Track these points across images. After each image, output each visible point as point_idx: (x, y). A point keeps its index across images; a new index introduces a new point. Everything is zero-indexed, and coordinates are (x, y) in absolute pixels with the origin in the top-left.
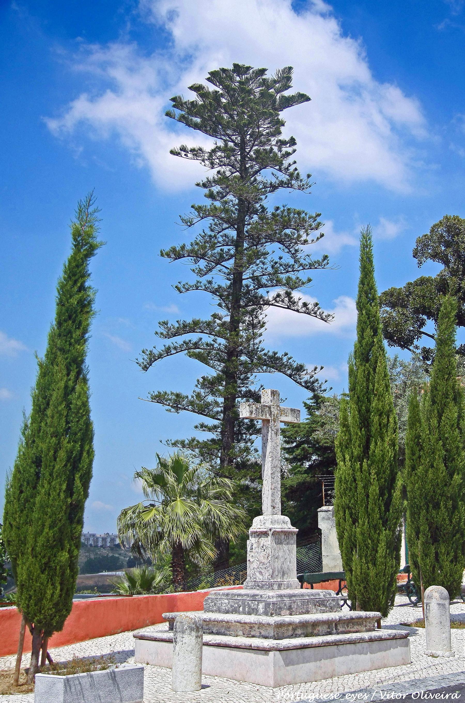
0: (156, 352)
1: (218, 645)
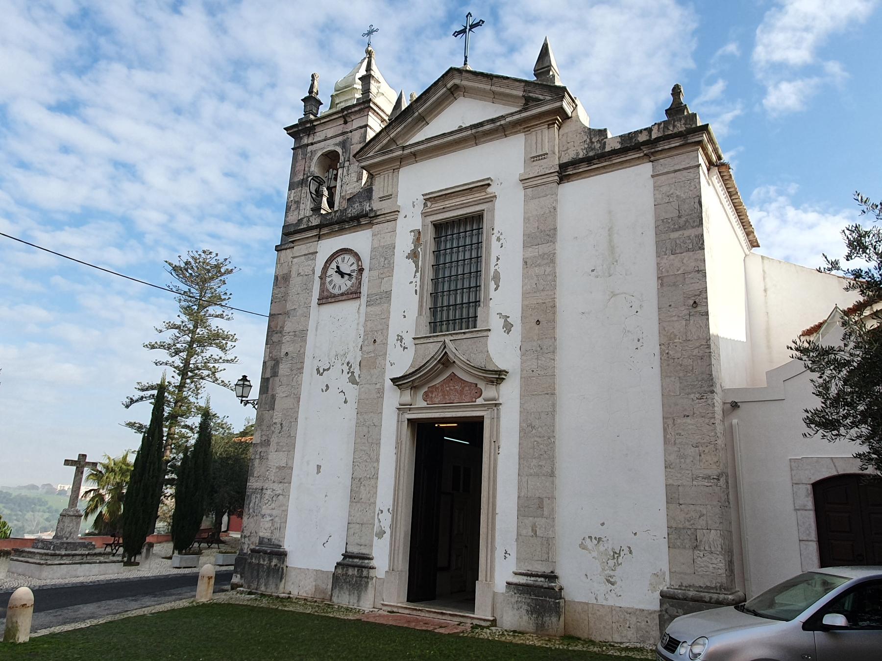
0: (134, 399)
1: (383, 111)
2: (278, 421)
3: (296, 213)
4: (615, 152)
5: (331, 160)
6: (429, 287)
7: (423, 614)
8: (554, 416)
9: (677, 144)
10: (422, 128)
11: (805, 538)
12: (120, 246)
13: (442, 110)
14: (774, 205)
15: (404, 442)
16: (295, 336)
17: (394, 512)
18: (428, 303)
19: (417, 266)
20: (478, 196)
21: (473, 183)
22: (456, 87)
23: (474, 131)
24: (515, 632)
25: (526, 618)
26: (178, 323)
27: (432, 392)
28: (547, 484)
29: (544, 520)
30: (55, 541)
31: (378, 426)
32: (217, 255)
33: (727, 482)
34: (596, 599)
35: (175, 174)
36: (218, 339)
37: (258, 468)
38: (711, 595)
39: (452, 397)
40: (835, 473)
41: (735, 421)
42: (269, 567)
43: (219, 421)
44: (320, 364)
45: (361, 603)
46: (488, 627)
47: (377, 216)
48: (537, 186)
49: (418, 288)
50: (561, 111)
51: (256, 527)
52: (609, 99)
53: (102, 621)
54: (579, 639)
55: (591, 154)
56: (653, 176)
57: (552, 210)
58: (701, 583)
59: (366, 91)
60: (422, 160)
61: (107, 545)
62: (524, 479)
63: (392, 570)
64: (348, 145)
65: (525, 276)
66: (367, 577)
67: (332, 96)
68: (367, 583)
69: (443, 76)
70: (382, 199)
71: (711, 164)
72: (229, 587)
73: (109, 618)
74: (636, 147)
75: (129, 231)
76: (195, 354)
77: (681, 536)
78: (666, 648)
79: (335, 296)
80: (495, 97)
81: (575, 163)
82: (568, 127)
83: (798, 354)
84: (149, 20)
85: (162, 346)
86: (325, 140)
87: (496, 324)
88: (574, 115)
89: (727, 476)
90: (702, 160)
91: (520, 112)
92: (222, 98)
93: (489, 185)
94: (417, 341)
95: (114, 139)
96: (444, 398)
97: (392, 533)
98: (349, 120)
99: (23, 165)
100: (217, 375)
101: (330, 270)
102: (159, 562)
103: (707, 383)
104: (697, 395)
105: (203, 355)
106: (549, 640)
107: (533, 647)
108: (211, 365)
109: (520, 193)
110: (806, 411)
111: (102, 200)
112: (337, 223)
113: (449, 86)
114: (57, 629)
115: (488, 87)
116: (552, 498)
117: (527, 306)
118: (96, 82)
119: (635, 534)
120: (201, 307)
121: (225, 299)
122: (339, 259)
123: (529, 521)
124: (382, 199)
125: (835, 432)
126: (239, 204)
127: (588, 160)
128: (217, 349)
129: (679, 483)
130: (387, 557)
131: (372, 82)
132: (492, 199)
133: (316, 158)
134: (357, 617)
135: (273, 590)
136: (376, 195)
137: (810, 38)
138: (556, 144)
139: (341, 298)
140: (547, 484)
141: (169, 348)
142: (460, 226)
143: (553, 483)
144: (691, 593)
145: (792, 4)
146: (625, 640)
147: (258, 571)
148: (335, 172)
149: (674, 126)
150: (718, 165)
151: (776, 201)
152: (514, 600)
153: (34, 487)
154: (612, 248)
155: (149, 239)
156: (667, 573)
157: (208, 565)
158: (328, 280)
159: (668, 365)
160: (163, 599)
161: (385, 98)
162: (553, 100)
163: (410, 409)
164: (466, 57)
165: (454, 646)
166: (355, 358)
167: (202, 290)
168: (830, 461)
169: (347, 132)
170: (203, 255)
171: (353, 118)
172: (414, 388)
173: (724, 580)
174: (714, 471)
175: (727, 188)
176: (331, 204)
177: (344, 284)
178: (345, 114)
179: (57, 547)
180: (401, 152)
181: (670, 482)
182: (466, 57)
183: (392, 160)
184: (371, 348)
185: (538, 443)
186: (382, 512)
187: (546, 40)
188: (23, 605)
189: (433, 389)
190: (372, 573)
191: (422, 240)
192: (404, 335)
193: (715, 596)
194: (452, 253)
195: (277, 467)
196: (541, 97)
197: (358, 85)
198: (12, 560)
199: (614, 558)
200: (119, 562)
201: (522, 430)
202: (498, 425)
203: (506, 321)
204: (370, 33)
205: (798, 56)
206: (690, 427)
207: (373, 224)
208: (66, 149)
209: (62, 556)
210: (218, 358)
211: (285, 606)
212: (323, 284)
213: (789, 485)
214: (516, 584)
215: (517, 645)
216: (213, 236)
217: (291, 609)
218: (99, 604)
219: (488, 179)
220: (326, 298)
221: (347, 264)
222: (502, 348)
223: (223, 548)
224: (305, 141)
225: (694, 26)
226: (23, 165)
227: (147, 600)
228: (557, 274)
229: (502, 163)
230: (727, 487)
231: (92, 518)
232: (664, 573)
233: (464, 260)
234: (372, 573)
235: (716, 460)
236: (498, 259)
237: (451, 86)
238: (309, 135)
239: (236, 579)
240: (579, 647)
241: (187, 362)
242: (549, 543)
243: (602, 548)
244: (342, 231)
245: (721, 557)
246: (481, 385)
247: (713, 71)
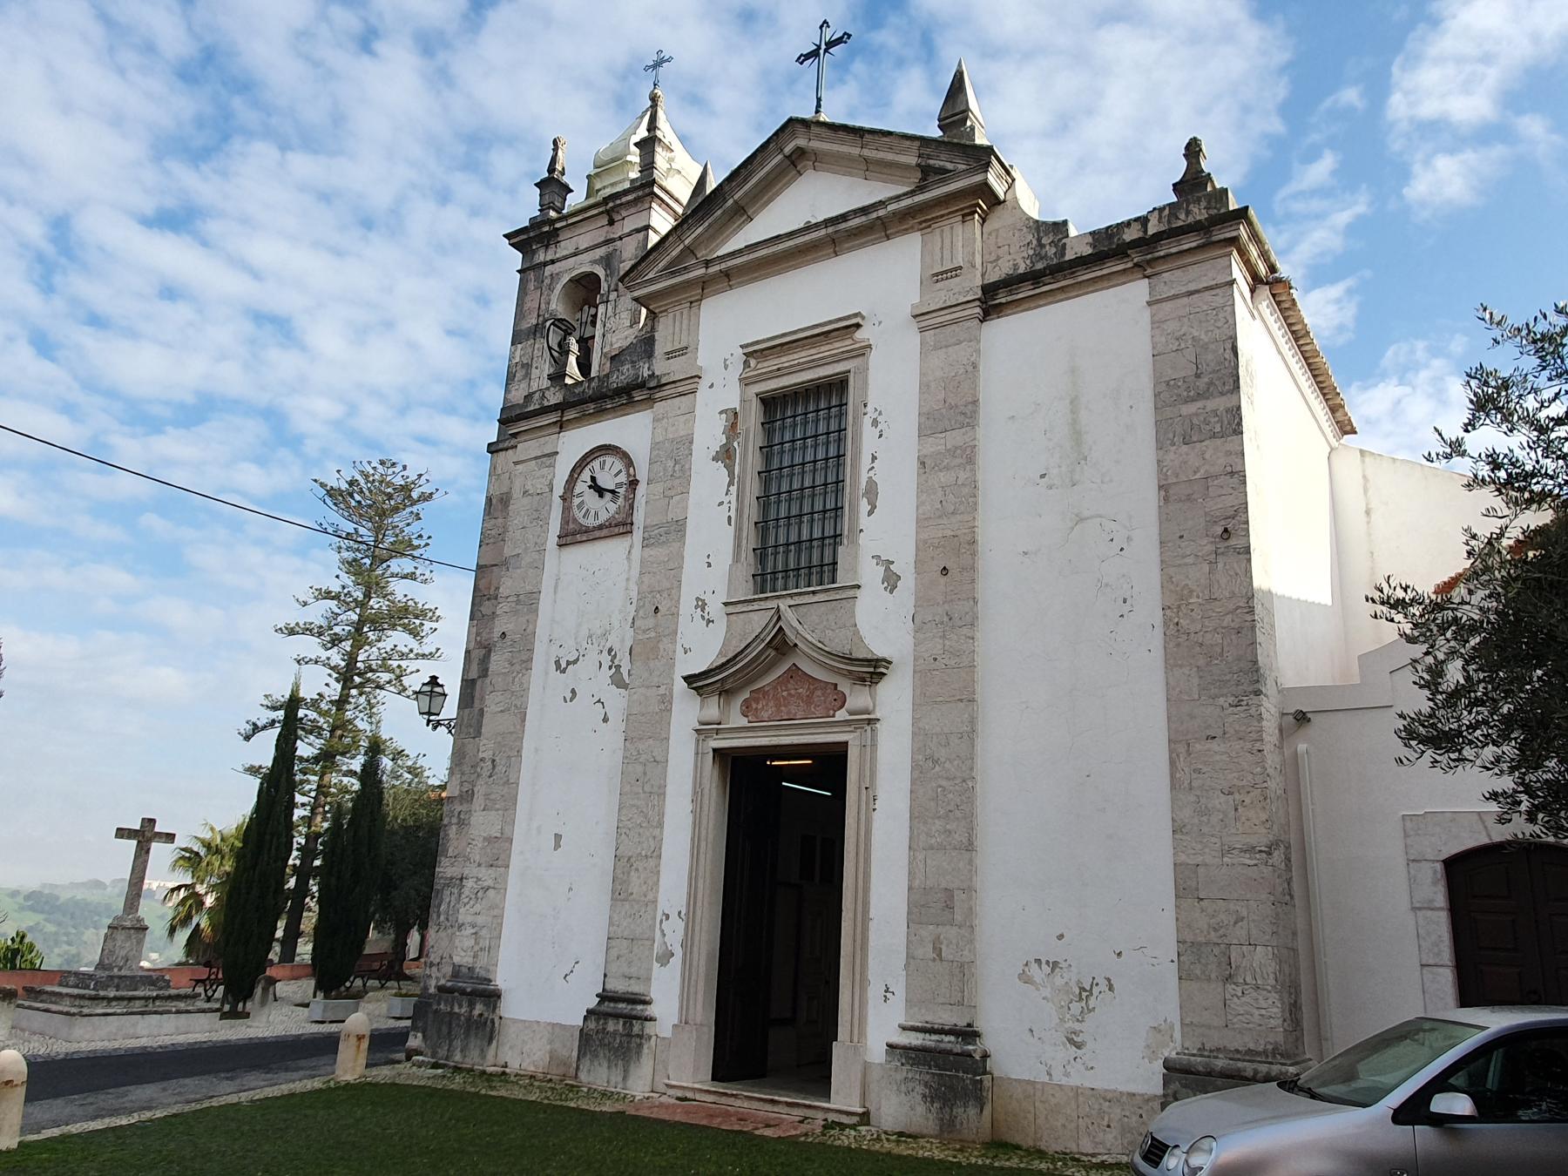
0: (260, 724)
1: (667, 192)
2: (487, 755)
3: (524, 385)
4: (1082, 262)
5: (586, 290)
6: (752, 512)
7: (738, 1103)
9: (1194, 245)
10: (740, 227)
11: (1431, 962)
12: (261, 461)
13: (777, 194)
14: (1424, 375)
15: (706, 791)
17: (690, 918)
18: (751, 540)
19: (731, 474)
21: (830, 322)
22: (800, 153)
23: (830, 230)
24: (901, 1134)
25: (921, 1109)
26: (335, 587)
28: (961, 865)
30: (100, 973)
31: (661, 763)
32: (405, 468)
33: (1288, 859)
34: (1049, 1074)
35: (360, 334)
36: (406, 617)
37: (453, 840)
38: (1255, 1065)
39: (793, 709)
40: (1486, 841)
41: (1302, 747)
42: (469, 1018)
43: (410, 763)
44: (561, 652)
45: (630, 1083)
46: (853, 1127)
47: (660, 386)
48: (943, 325)
49: (733, 514)
50: (985, 190)
51: (448, 946)
52: (1071, 169)
53: (159, 1114)
54: (1018, 1147)
55: (1039, 266)
56: (1149, 304)
57: (970, 369)
59: (648, 166)
60: (741, 284)
61: (198, 981)
62: (920, 856)
63: (685, 1021)
65: (921, 490)
66: (640, 1036)
67: (588, 177)
68: (640, 1046)
69: (776, 134)
70: (670, 355)
71: (1256, 281)
72: (401, 1056)
73: (175, 1110)
74: (1120, 251)
75: (279, 432)
76: (366, 643)
77: (1204, 959)
78: (1145, 1158)
79: (587, 530)
80: (869, 168)
81: (1011, 282)
82: (998, 220)
83: (1385, 609)
84: (317, 64)
85: (308, 630)
86: (576, 254)
87: (870, 575)
88: (1009, 197)
89: (1288, 847)
90: (1238, 272)
91: (912, 193)
92: (444, 197)
93: (858, 326)
94: (731, 609)
95: (256, 275)
96: (779, 711)
97: (685, 954)
98: (617, 217)
99: (96, 321)
100: (406, 681)
101: (579, 483)
102: (286, 1011)
103: (1248, 676)
104: (1231, 699)
105: (380, 645)
106: (961, 1150)
107: (929, 1161)
108: (395, 664)
110: (1402, 716)
111: (232, 379)
112: (592, 400)
113: (787, 150)
114: (74, 1129)
115: (856, 151)
116: (969, 890)
117: (925, 542)
118: (224, 174)
119: (1119, 954)
120: (378, 560)
121: (418, 547)
122: (596, 464)
123: (927, 932)
124: (670, 355)
125: (1453, 756)
126: (472, 384)
127: (1033, 277)
128: (406, 636)
129: (1199, 859)
130: (677, 999)
131: (658, 149)
132: (863, 351)
133: (559, 287)
134: (619, 1107)
135: (477, 1060)
136: (660, 348)
137: (1493, 76)
138: (975, 249)
139: (597, 534)
140: (961, 865)
141: (320, 634)
142: (808, 402)
143: (971, 862)
144: (1220, 1063)
145: (1454, 17)
147: (450, 1024)
148: (593, 311)
149: (1188, 213)
150: (1269, 283)
151: (1427, 366)
152: (900, 1076)
153: (98, 884)
154: (1077, 435)
155: (311, 448)
156: (1177, 1027)
157: (366, 1016)
158: (576, 501)
159: (1178, 645)
160: (283, 1075)
161: (679, 177)
162: (970, 172)
163: (718, 731)
164: (819, 100)
165: (782, 1159)
166: (623, 641)
167: (378, 530)
168: (1476, 817)
169: (613, 240)
170: (380, 469)
171: (624, 213)
172: (726, 692)
173: (1280, 1038)
174: (1261, 838)
175: (1289, 325)
176: (584, 366)
177: (605, 509)
178: (609, 208)
179: (101, 985)
180: (703, 271)
181: (1183, 858)
182: (819, 100)
183: (688, 285)
184: (651, 622)
185: (944, 789)
186: (668, 917)
187: (960, 64)
188: (8, 1083)
190: (649, 1028)
191: (740, 427)
192: (708, 598)
194: (793, 450)
196: (949, 166)
197: (634, 157)
198: (19, 1006)
199: (1081, 999)
200: (217, 1010)
201: (915, 766)
202: (873, 760)
203: (887, 569)
204: (657, 65)
205: (1471, 107)
206: (1218, 758)
207: (654, 401)
208: (170, 292)
209: (110, 1000)
210: (406, 650)
211: (492, 1088)
212: (567, 509)
213: (1402, 861)
214: (904, 1048)
215: (899, 1157)
216: (424, 440)
217: (503, 1093)
218: (165, 1084)
219: (856, 315)
220: (573, 535)
221: (609, 473)
222: (880, 619)
223: (407, 986)
224: (541, 256)
225: (1284, 57)
226: (96, 321)
227: (252, 1079)
228: (980, 484)
229: (882, 286)
230: (1289, 868)
231: (183, 936)
232: (1172, 1027)
233: (815, 462)
234: (649, 1028)
235: (1264, 817)
236: (874, 458)
237: (789, 150)
238: (547, 247)
239: (415, 1041)
240: (1014, 1162)
241: (351, 659)
243: (1059, 981)
244: (600, 414)
245: (1274, 997)
246: (845, 686)
247: (1315, 137)
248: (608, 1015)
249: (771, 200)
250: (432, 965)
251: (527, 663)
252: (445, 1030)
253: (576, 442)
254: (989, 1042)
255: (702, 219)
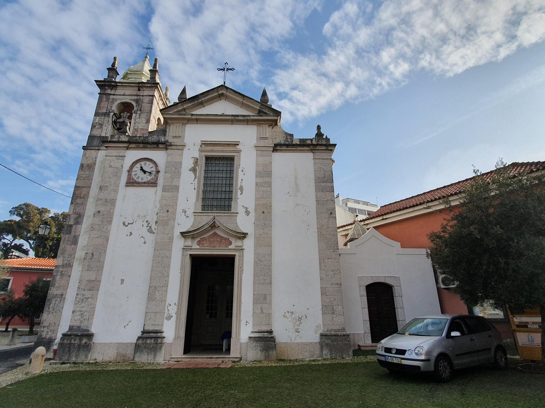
7: (198, 360)
8: (271, 256)
13: (213, 103)
16: (106, 201)
17: (179, 305)
19: (196, 176)
20: (231, 148)
22: (222, 94)
23: (233, 118)
25: (260, 353)
27: (203, 241)
29: (266, 305)
45: (157, 359)
46: (238, 362)
47: (171, 145)
49: (196, 187)
55: (287, 143)
58: (335, 328)
59: (153, 78)
60: (201, 124)
62: (257, 286)
63: (176, 338)
64: (140, 102)
65: (256, 191)
68: (161, 346)
69: (217, 87)
70: (174, 137)
74: (304, 145)
77: (328, 309)
79: (139, 183)
80: (243, 105)
82: (275, 129)
87: (241, 211)
93: (238, 144)
94: (195, 214)
98: (141, 89)
109: (254, 152)
112: (143, 143)
113: (220, 92)
123: (259, 306)
127: (284, 145)
130: (173, 331)
132: (239, 151)
135: (83, 359)
144: (333, 333)
146: (304, 357)
154: (297, 185)
163: (191, 249)
169: (140, 96)
171: (144, 89)
172: (193, 238)
177: (146, 178)
181: (323, 286)
184: (165, 214)
186: (170, 305)
189: (203, 239)
191: (199, 163)
193: (342, 333)
195: (87, 281)
203: (246, 210)
213: (358, 286)
214: (254, 337)
220: (131, 183)
221: (148, 167)
222: (244, 222)
229: (246, 137)
236: (242, 180)
237: (220, 93)
238: (112, 89)
242: (269, 316)
243: (293, 317)
244: (145, 148)
246: (231, 239)
248: (147, 338)
249: (211, 104)
250: (44, 327)
251: (110, 222)
252: (67, 349)
253: (133, 155)
254: (275, 334)
255: (191, 102)
